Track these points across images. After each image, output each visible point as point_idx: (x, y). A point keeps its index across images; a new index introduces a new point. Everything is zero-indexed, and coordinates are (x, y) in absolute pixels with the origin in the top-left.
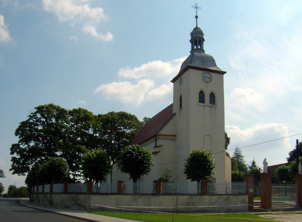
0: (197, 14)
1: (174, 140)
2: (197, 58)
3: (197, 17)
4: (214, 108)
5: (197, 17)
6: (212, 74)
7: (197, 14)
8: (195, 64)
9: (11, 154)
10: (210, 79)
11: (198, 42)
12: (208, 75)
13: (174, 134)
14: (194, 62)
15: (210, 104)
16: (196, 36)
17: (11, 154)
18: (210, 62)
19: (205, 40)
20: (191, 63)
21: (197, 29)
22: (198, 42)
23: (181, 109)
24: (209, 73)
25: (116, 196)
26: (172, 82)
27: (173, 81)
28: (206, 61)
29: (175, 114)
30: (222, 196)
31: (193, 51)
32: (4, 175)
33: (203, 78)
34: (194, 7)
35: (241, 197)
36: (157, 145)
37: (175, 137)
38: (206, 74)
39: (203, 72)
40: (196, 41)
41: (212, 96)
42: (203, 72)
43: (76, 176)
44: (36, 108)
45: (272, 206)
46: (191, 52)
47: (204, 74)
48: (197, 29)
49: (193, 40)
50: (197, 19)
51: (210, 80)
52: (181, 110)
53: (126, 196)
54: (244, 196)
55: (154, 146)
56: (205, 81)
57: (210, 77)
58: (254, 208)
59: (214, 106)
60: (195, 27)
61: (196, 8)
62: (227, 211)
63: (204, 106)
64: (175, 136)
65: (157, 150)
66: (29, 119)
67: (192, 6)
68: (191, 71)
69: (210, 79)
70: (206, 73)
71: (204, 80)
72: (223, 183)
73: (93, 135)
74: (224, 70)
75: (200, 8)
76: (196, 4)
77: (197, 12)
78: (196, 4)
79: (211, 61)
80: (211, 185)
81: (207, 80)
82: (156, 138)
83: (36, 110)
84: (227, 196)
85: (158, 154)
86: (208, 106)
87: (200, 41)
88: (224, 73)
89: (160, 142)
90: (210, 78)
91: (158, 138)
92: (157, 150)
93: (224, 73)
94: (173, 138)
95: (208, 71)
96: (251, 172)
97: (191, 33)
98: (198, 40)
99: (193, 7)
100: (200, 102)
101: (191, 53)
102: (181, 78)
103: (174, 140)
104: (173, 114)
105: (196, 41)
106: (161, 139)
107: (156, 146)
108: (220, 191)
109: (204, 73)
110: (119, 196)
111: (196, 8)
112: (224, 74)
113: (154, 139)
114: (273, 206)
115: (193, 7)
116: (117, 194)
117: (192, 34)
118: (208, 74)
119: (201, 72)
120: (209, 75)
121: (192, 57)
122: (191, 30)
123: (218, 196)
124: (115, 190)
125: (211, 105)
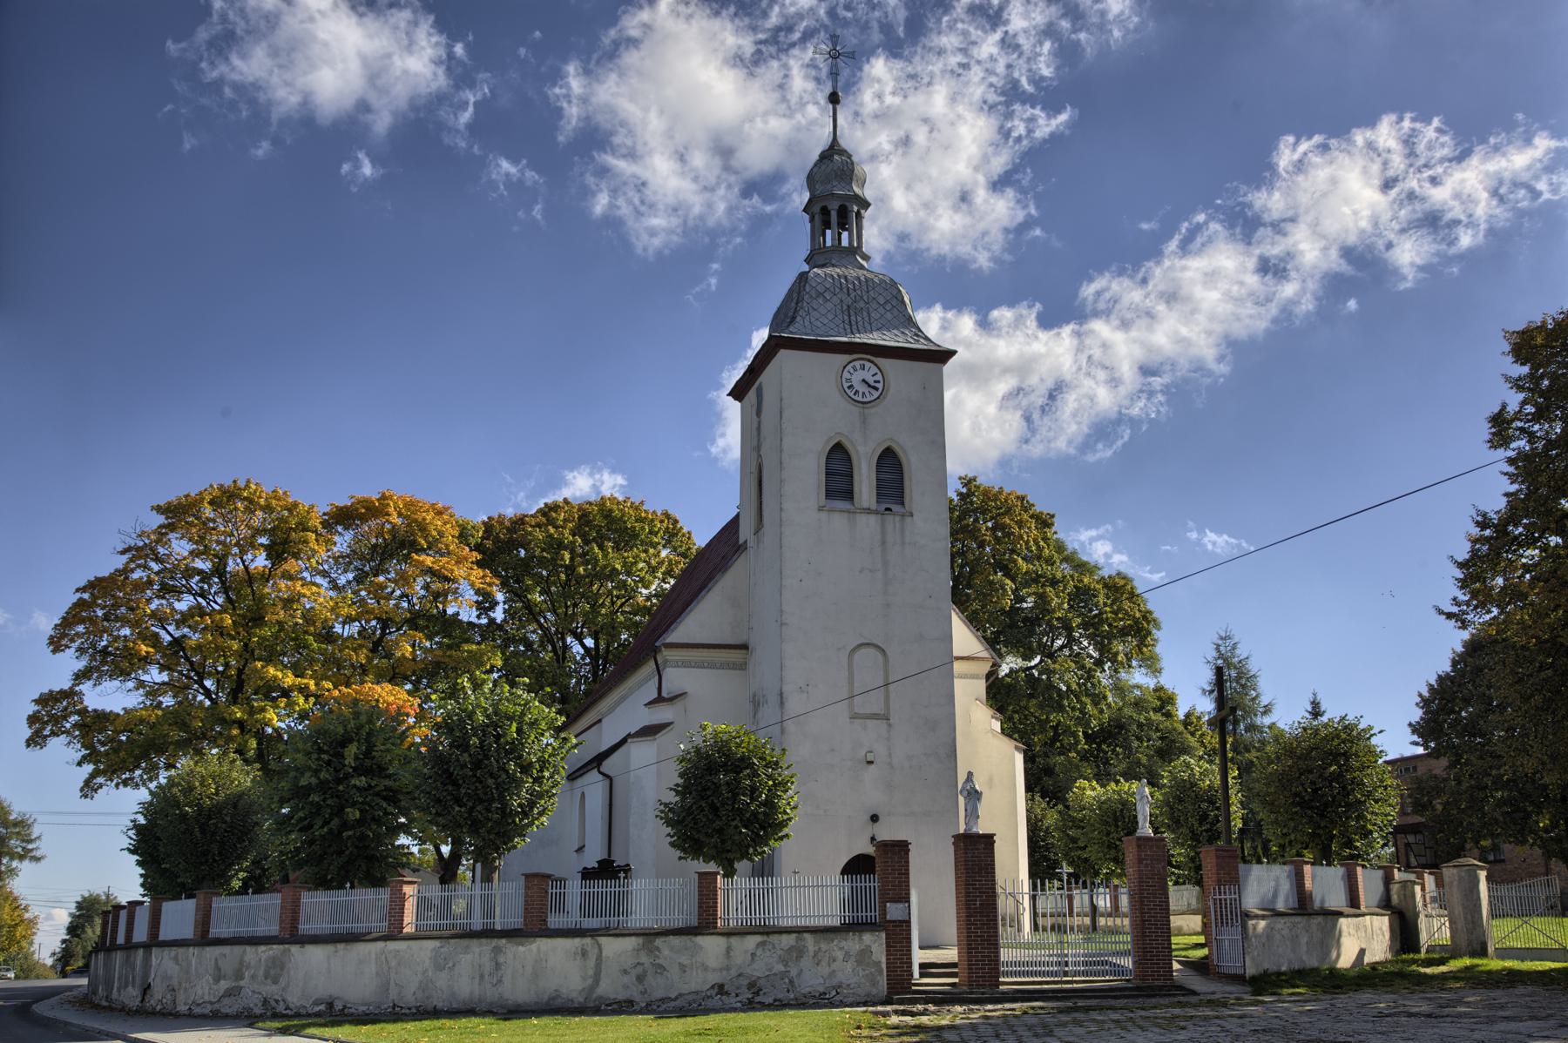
1: (742, 667)
2: (820, 294)
6: (884, 363)
8: (818, 322)
9: (28, 746)
10: (877, 389)
11: (834, 215)
12: (869, 373)
13: (738, 642)
17: (28, 746)
18: (881, 310)
21: (833, 151)
22: (834, 215)
24: (872, 362)
26: (736, 398)
28: (862, 304)
30: (774, 938)
35: (853, 943)
36: (664, 694)
37: (744, 651)
38: (858, 367)
39: (842, 359)
41: (889, 462)
44: (158, 509)
45: (1001, 979)
47: (849, 367)
48: (833, 151)
49: (817, 208)
51: (876, 394)
54: (867, 938)
56: (856, 398)
57: (878, 377)
58: (913, 988)
62: (1270, 1030)
64: (744, 647)
65: (662, 714)
66: (161, 534)
69: (877, 389)
70: (857, 364)
71: (851, 394)
73: (1328, 138)
79: (887, 302)
81: (857, 392)
82: (660, 660)
83: (161, 519)
84: (794, 936)
86: (868, 511)
87: (843, 213)
89: (675, 679)
90: (880, 386)
92: (662, 714)
95: (867, 354)
96: (79, 917)
98: (834, 207)
101: (808, 263)
102: (760, 384)
103: (742, 667)
105: (825, 211)
107: (660, 700)
113: (650, 667)
114: (1007, 980)
118: (868, 365)
120: (874, 369)
121: (799, 293)
123: (758, 938)
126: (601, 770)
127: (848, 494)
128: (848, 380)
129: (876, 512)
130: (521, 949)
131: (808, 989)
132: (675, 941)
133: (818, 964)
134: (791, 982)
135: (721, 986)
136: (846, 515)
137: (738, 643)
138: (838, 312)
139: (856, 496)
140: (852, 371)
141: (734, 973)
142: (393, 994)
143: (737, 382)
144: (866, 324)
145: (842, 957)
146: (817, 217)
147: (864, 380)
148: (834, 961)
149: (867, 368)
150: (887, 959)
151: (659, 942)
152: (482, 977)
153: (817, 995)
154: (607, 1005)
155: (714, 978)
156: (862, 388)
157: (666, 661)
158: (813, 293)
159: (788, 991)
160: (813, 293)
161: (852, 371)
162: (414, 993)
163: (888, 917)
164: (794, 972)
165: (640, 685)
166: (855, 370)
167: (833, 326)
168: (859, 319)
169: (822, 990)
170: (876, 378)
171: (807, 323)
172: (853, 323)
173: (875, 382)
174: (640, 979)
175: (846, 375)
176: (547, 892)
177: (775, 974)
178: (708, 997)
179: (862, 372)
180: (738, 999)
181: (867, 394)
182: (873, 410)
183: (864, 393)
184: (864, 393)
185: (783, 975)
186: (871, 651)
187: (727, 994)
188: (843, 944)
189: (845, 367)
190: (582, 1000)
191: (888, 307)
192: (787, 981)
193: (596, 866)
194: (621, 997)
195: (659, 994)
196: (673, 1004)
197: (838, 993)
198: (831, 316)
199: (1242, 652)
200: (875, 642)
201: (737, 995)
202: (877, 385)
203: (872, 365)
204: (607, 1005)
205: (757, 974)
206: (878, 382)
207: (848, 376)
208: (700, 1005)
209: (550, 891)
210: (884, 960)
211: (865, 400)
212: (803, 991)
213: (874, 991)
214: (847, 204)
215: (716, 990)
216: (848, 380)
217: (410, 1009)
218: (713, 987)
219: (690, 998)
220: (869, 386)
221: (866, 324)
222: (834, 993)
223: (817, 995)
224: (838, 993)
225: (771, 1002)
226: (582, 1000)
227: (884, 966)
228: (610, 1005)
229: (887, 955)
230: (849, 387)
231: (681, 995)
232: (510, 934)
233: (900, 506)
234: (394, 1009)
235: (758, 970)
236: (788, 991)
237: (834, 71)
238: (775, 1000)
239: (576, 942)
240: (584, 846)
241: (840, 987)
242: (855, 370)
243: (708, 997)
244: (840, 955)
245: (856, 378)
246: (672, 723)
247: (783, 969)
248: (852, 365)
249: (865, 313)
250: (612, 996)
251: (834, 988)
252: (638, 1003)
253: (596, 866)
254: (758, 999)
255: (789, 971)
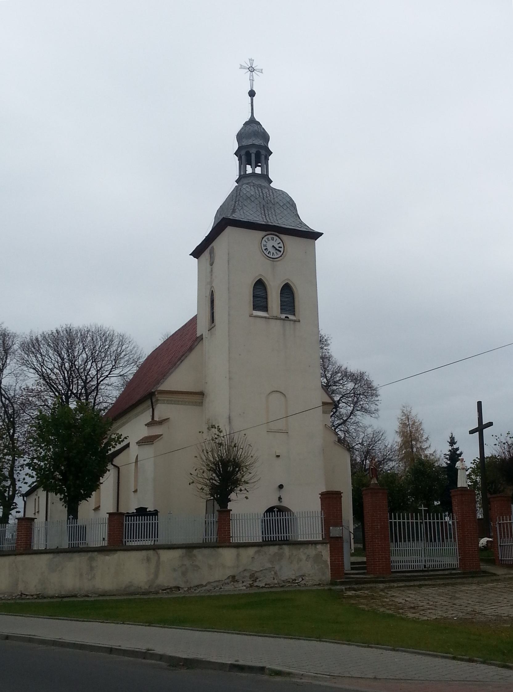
0: (252, 85)
1: (201, 404)
3: (252, 94)
4: (292, 322)
5: (252, 94)
6: (284, 237)
7: (252, 85)
10: (280, 251)
13: (197, 390)
14: (242, 208)
15: (281, 313)
16: (250, 142)
19: (272, 151)
20: (234, 211)
21: (252, 122)
23: (213, 325)
25: (12, 558)
27: (197, 253)
28: (271, 205)
29: (201, 338)
31: (242, 177)
32: (162, 338)
33: (264, 248)
34: (245, 68)
36: (156, 419)
38: (270, 239)
39: (261, 234)
40: (248, 154)
42: (264, 233)
43: (353, 458)
46: (237, 181)
47: (265, 238)
48: (252, 122)
49: (243, 152)
50: (254, 98)
51: (280, 254)
52: (213, 327)
53: (35, 557)
55: (150, 420)
56: (269, 255)
57: (281, 245)
59: (291, 317)
60: (247, 118)
61: (252, 70)
63: (265, 318)
65: (156, 431)
67: (241, 65)
68: (229, 231)
69: (280, 251)
70: (270, 237)
71: (267, 254)
72: (62, 521)
74: (317, 229)
75: (262, 70)
76: (251, 60)
77: (252, 80)
78: (251, 60)
80: (3, 530)
81: (269, 252)
85: (158, 444)
86: (277, 318)
87: (258, 155)
88: (316, 235)
90: (282, 250)
91: (157, 400)
93: (316, 235)
94: (197, 398)
97: (238, 134)
98: (253, 151)
99: (242, 67)
100: (255, 308)
102: (213, 247)
104: (198, 338)
105: (248, 154)
106: (163, 402)
107: (152, 423)
108: (309, 518)
109: (265, 236)
110: (20, 558)
111: (252, 70)
112: (316, 240)
113: (149, 402)
115: (242, 67)
116: (15, 555)
117: (240, 136)
118: (275, 238)
119: (259, 234)
120: (279, 241)
122: (239, 126)
124: (214, 538)
125: (283, 316)
126: (114, 463)
127: (265, 308)
128: (265, 245)
129: (281, 319)
130: (107, 558)
131: (286, 578)
132: (206, 551)
133: (291, 563)
134: (276, 573)
135: (233, 577)
136: (264, 319)
137: (197, 391)
138: (258, 208)
139: (269, 309)
140: (267, 241)
141: (241, 569)
142: (21, 588)
143: (197, 247)
144: (274, 216)
145: (305, 559)
146: (243, 157)
147: (273, 246)
148: (301, 561)
149: (275, 240)
150: (330, 559)
151: (196, 552)
152: (81, 575)
153: (291, 581)
154: (163, 590)
155: (229, 573)
156: (272, 250)
157: (157, 400)
158: (245, 197)
159: (274, 579)
160: (245, 197)
161: (267, 241)
162: (35, 586)
163: (331, 535)
164: (277, 568)
165: (142, 412)
166: (269, 240)
167: (256, 216)
168: (270, 213)
169: (293, 578)
170: (280, 245)
171: (242, 213)
172: (267, 215)
173: (279, 247)
174: (184, 574)
175: (264, 243)
176: (123, 524)
177: (266, 569)
178: (226, 584)
179: (272, 242)
180: (244, 584)
181: (275, 253)
182: (278, 263)
183: (273, 253)
184: (273, 253)
185: (270, 569)
186: (278, 395)
187: (237, 581)
188: (306, 551)
189: (263, 238)
190: (147, 587)
191: (285, 207)
192: (273, 573)
193: (135, 511)
194: (172, 585)
195: (196, 582)
196: (204, 588)
197: (303, 580)
198: (254, 210)
199: (413, 413)
200: (280, 390)
201: (243, 582)
202: (280, 249)
203: (277, 238)
204: (163, 590)
205: (255, 569)
206: (281, 247)
207: (265, 243)
208: (221, 588)
209: (125, 523)
210: (329, 560)
211: (274, 257)
212: (282, 579)
213: (324, 578)
214: (260, 150)
215: (230, 579)
216: (265, 245)
217: (32, 596)
218: (228, 578)
219: (215, 584)
220: (276, 249)
221: (274, 216)
222: (300, 579)
223: (291, 581)
224: (303, 580)
225: (264, 585)
226: (147, 587)
227: (329, 563)
228: (165, 590)
229: (330, 557)
230: (265, 250)
231: (209, 583)
232: (101, 550)
233: (292, 316)
234: (21, 596)
235: (256, 567)
236: (274, 579)
237: (251, 78)
238: (266, 585)
239: (144, 553)
240: (99, 506)
241: (303, 576)
242: (269, 240)
243: (226, 584)
244: (304, 557)
245: (270, 245)
246: (162, 435)
247: (271, 566)
248: (267, 237)
249: (273, 211)
250: (166, 585)
251: (301, 576)
252: (183, 588)
253: (135, 511)
254: (256, 584)
255: (274, 567)
